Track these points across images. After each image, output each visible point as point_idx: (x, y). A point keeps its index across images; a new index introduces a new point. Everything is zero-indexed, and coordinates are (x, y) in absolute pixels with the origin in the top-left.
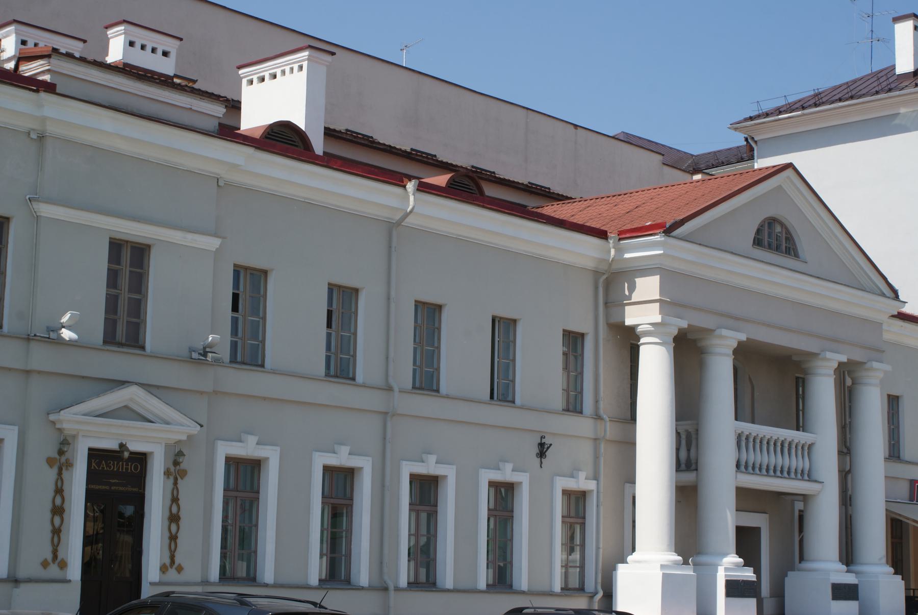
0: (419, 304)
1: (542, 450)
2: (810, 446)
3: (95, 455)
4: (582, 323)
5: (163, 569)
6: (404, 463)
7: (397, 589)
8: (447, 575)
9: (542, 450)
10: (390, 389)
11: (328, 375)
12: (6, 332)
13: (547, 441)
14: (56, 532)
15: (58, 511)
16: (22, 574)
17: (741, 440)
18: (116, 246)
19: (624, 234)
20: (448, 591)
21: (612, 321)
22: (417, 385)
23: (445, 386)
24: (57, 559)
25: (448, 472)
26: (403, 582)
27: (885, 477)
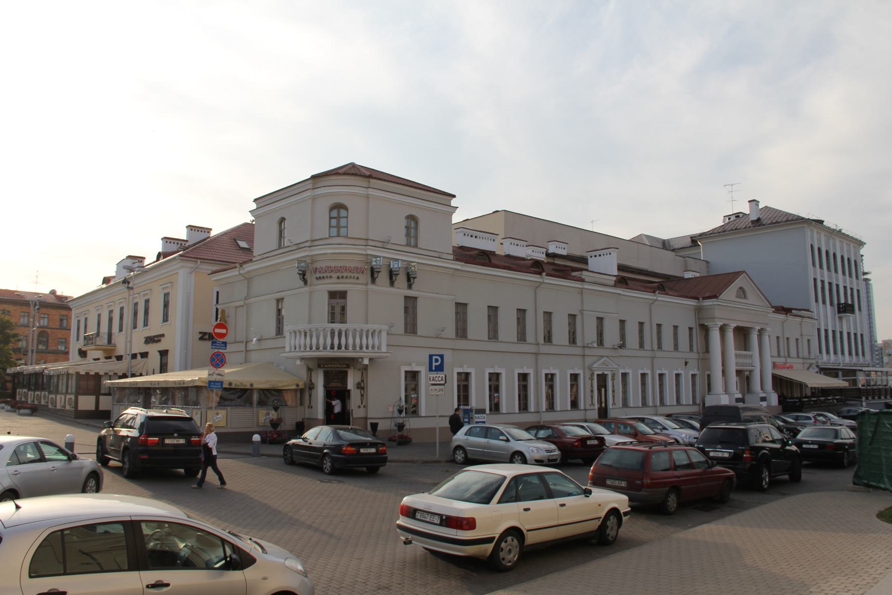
0: (657, 324)
1: (686, 363)
2: (752, 355)
3: (598, 375)
4: (780, 335)
5: (612, 405)
6: (402, 366)
7: (543, 412)
8: (504, 408)
9: (686, 363)
10: (538, 344)
11: (406, 331)
12: (826, 360)
13: (687, 361)
14: (592, 397)
15: (592, 391)
16: (587, 408)
17: (736, 355)
18: (598, 318)
19: (704, 298)
20: (631, 407)
21: (700, 323)
22: (491, 337)
23: (469, 337)
24: (593, 404)
25: (502, 371)
26: (544, 410)
27: (387, 345)
